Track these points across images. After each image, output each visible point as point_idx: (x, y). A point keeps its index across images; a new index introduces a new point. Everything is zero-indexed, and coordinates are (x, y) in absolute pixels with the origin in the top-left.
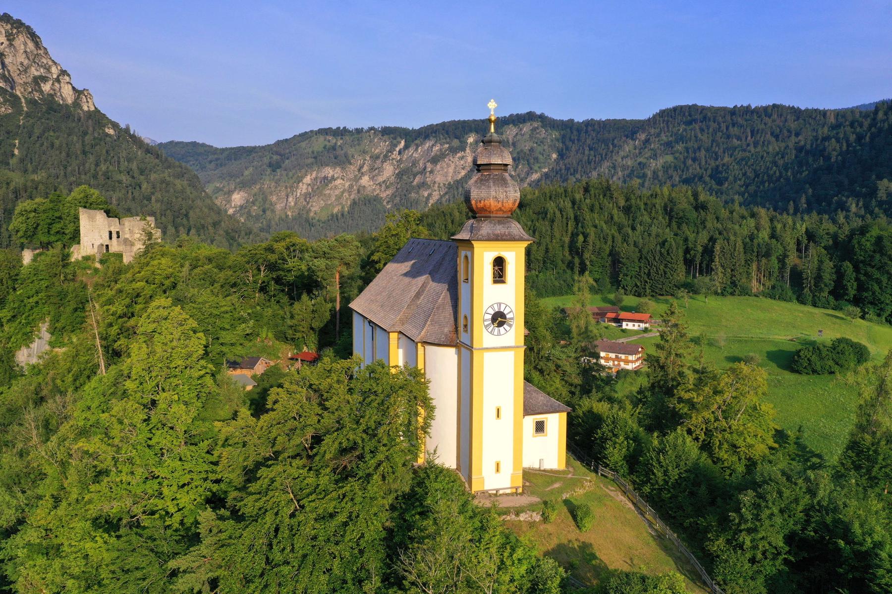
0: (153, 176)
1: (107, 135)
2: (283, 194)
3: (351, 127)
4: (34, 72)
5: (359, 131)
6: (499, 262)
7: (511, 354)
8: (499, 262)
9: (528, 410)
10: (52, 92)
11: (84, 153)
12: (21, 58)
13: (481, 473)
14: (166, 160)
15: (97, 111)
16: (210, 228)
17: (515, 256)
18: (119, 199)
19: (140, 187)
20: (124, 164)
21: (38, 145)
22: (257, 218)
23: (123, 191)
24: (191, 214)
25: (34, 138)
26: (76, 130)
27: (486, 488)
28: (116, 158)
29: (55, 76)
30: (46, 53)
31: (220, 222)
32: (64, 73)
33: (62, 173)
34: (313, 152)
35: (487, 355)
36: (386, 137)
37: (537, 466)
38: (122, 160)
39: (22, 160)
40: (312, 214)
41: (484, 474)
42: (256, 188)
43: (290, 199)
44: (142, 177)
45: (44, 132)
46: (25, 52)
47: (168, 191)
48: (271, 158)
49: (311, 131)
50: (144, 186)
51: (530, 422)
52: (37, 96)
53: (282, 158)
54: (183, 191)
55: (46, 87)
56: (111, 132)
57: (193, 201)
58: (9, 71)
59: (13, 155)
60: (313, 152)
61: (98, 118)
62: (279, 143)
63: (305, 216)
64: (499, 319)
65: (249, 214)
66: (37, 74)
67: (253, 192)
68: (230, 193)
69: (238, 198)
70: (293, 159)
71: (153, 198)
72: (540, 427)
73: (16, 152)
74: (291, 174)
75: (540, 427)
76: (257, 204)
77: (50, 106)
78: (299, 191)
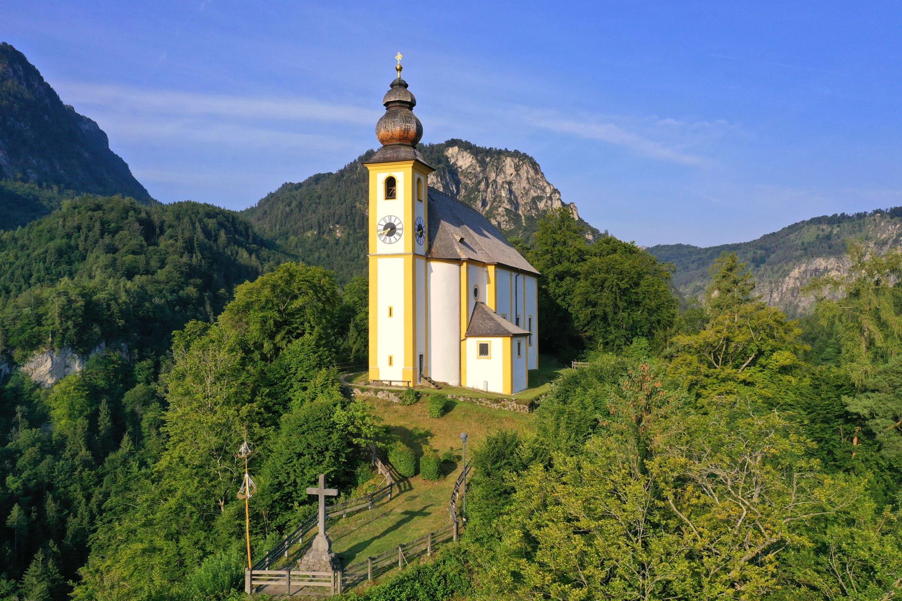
2: (767, 290)
3: (850, 212)
4: (533, 193)
5: (861, 216)
6: (391, 183)
7: (400, 261)
8: (391, 183)
9: (472, 332)
12: (524, 184)
27: (381, 379)
30: (543, 177)
32: (555, 191)
34: (803, 244)
35: (380, 261)
36: (896, 219)
37: (481, 387)
40: (800, 310)
43: (775, 295)
46: (527, 178)
48: (755, 253)
49: (803, 222)
51: (472, 344)
53: (769, 252)
55: (541, 205)
56: (590, 237)
60: (803, 244)
62: (765, 237)
64: (391, 229)
66: (535, 195)
70: (780, 252)
72: (484, 350)
74: (776, 268)
75: (484, 350)
78: (785, 286)
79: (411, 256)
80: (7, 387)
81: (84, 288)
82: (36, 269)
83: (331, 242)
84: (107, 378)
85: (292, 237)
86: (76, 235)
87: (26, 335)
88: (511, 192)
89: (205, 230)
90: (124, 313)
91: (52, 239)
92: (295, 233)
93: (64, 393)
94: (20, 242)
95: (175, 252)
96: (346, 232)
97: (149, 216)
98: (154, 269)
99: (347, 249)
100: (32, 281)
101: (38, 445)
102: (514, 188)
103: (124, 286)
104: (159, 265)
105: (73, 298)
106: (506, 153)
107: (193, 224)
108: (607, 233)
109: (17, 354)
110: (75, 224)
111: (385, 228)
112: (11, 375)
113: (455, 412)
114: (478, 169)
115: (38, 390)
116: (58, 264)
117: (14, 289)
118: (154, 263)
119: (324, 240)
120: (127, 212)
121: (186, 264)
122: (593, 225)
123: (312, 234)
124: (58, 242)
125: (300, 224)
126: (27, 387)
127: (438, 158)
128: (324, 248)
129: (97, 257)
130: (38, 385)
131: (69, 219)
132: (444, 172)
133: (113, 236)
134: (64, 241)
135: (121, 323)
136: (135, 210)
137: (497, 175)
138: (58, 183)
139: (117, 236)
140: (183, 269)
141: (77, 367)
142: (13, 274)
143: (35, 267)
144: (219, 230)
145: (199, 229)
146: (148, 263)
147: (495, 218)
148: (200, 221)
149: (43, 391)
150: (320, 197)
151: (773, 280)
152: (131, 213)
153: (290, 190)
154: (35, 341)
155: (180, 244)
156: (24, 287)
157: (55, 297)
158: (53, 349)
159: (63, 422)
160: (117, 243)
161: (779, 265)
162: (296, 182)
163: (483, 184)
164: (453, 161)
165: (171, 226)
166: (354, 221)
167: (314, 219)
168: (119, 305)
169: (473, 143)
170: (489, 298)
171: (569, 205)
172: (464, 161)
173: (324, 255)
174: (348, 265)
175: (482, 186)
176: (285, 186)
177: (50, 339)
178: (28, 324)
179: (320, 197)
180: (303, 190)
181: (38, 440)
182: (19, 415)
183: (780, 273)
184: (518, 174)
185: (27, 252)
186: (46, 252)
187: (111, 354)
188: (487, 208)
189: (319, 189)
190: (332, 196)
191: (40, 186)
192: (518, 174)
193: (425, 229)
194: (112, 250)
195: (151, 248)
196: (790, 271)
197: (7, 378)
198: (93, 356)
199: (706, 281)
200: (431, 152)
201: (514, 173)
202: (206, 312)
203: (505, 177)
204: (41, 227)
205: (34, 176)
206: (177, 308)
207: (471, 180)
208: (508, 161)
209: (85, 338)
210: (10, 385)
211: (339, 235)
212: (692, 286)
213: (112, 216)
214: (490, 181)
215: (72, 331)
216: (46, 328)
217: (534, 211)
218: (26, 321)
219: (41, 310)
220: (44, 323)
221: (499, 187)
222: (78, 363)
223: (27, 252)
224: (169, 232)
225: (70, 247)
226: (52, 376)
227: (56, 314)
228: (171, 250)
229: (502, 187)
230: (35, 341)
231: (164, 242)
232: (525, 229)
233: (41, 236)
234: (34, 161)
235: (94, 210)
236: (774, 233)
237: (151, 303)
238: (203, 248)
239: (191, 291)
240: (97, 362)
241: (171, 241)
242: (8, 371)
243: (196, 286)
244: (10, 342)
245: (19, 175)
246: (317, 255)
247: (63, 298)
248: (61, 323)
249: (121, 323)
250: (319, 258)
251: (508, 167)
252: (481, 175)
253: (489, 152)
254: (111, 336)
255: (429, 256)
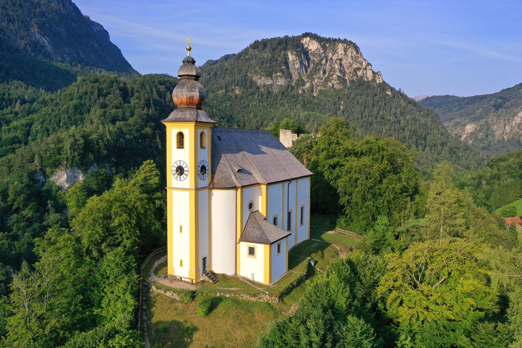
0: (408, 117)
1: (388, 95)
4: (355, 66)
6: (181, 136)
8: (181, 136)
9: (244, 238)
10: (362, 75)
11: (373, 105)
12: (350, 60)
13: (172, 264)
14: (420, 107)
15: (384, 82)
16: (439, 146)
17: (189, 131)
18: (386, 130)
19: (400, 123)
20: (393, 110)
21: (351, 103)
22: (482, 140)
23: (390, 125)
24: (428, 137)
25: (350, 99)
26: (371, 94)
28: (389, 108)
29: (364, 67)
30: (361, 55)
31: (447, 142)
32: (369, 64)
33: (360, 116)
35: (175, 192)
37: (250, 277)
38: (392, 108)
39: (343, 112)
41: (174, 265)
42: (482, 122)
43: (507, 128)
44: (402, 117)
45: (355, 96)
46: (352, 56)
47: (415, 125)
48: (496, 101)
50: (402, 122)
51: (244, 246)
52: (355, 78)
54: (426, 124)
55: (360, 73)
56: (389, 93)
57: (431, 130)
58: (343, 68)
59: (340, 109)
61: (384, 86)
62: (503, 91)
63: (517, 139)
64: (180, 170)
65: (476, 138)
66: (356, 67)
67: (480, 124)
68: (465, 125)
69: (470, 128)
70: (512, 101)
71: (406, 129)
72: (252, 251)
73: (341, 107)
75: (252, 251)
76: (483, 131)
77: (361, 84)
78: (514, 122)
79: (194, 191)
80: (43, 189)
81: (84, 132)
82: (63, 118)
83: (233, 97)
84: (98, 184)
85: (210, 94)
86: (84, 97)
87: (52, 160)
88: (341, 65)
89: (158, 92)
90: (107, 147)
91: (71, 100)
92: (212, 92)
93: (74, 193)
94: (55, 102)
95: (139, 107)
96: (242, 91)
97: (125, 86)
98: (127, 117)
99: (242, 101)
100: (61, 124)
101: (60, 223)
102: (343, 62)
103: (108, 129)
104: (130, 115)
105: (77, 138)
106: (339, 41)
107: (151, 88)
108: (400, 90)
109: (48, 170)
110: (84, 91)
111: (177, 171)
112: (46, 182)
113: (220, 309)
114: (322, 51)
115: (60, 191)
116: (75, 114)
117: (51, 129)
118: (127, 114)
119: (229, 95)
120: (113, 83)
121: (145, 114)
122: (392, 85)
123: (222, 92)
124: (75, 101)
125: (215, 86)
126: (54, 189)
127: (297, 45)
128: (229, 100)
129: (96, 111)
130: (60, 188)
131: (81, 88)
132: (301, 54)
133: (105, 98)
134: (78, 101)
135: (105, 152)
136: (117, 82)
137: (333, 55)
138: (81, 63)
139: (107, 98)
140: (144, 117)
141: (81, 178)
142: (50, 120)
143: (62, 117)
144: (166, 92)
145: (155, 92)
146: (124, 113)
147: (331, 82)
148: (156, 87)
149: (63, 192)
150: (227, 70)
151: (506, 118)
152: (115, 84)
153: (211, 65)
154: (57, 163)
155: (143, 101)
156: (56, 128)
157: (68, 136)
158: (67, 168)
159: (74, 209)
160: (107, 102)
161: (512, 109)
162: (215, 60)
163: (324, 60)
164: (306, 46)
165: (137, 91)
166: (246, 84)
167: (223, 82)
168: (103, 142)
169: (319, 35)
170: (261, 206)
171: (377, 73)
172: (313, 46)
173: (228, 105)
174: (242, 111)
175: (324, 61)
176: (208, 62)
177: (65, 162)
178: (53, 154)
179: (227, 70)
180: (218, 65)
181: (60, 220)
182: (50, 205)
183: (511, 114)
184: (346, 54)
185: (59, 107)
186: (68, 107)
187: (100, 170)
188: (326, 75)
189: (226, 64)
190: (234, 69)
191: (71, 64)
192: (346, 54)
193: (208, 168)
194: (104, 106)
195: (126, 105)
196: (518, 113)
197: (43, 184)
198: (89, 171)
199: (463, 119)
200: (293, 41)
201: (344, 53)
202: (157, 142)
203: (338, 56)
204: (66, 93)
205: (68, 59)
206: (140, 141)
207: (317, 58)
208: (340, 46)
209: (85, 161)
210: (45, 188)
211: (237, 92)
212: (453, 122)
213: (104, 86)
214: (328, 59)
215: (77, 158)
216: (62, 156)
217: (355, 77)
218: (52, 152)
219: (60, 145)
220: (62, 153)
221: (334, 62)
222: (81, 175)
223: (59, 107)
224: (136, 94)
225: (81, 104)
226: (67, 183)
227: (68, 148)
228: (137, 105)
229: (336, 62)
230: (57, 163)
231: (133, 101)
232: (349, 88)
233: (66, 98)
234: (67, 50)
235: (94, 82)
236: (510, 88)
237: (125, 139)
238: (156, 102)
239: (148, 130)
240: (92, 175)
241: (138, 100)
242: (44, 180)
243: (151, 127)
244: (43, 164)
245: (60, 59)
246: (224, 105)
247: (72, 139)
248: (71, 153)
249: (105, 152)
250: (226, 106)
251: (340, 49)
252: (323, 55)
253: (328, 40)
254: (99, 160)
255: (212, 186)
